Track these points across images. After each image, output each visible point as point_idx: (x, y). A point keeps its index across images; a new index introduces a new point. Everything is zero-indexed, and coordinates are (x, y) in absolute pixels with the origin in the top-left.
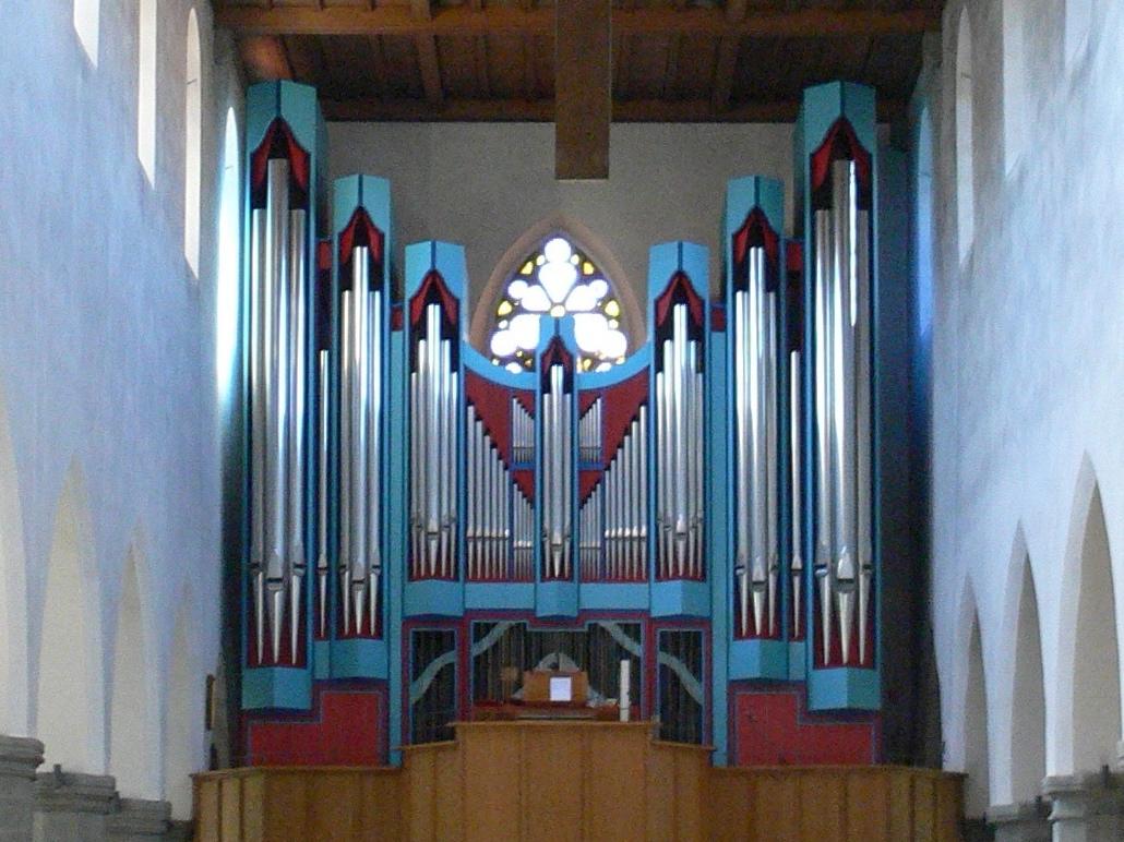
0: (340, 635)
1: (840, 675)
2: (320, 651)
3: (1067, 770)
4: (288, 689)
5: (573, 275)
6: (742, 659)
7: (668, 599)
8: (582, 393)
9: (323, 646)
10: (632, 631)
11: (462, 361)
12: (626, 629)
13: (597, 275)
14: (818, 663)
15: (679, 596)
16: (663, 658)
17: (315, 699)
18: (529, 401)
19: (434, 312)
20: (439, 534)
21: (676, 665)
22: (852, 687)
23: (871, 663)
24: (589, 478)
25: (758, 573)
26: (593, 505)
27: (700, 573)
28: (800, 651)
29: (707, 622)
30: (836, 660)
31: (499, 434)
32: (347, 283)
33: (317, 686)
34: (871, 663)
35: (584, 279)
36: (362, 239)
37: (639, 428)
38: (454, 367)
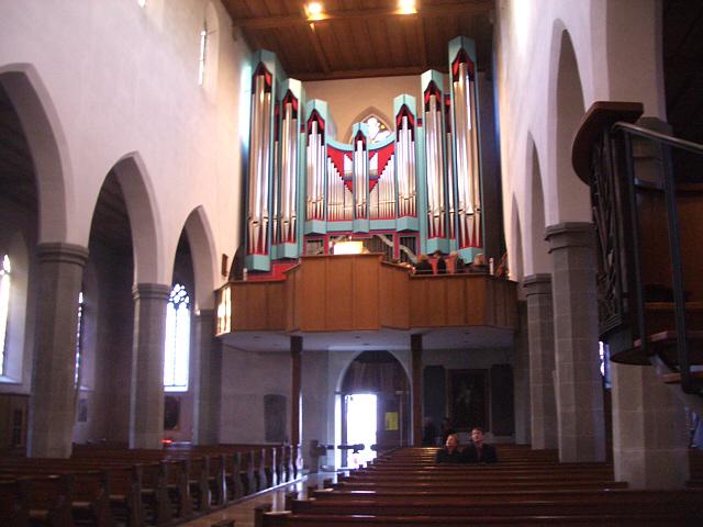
0: (281, 242)
1: (469, 250)
2: (273, 249)
3: (531, 273)
4: (261, 262)
5: (378, 129)
6: (430, 246)
7: (402, 224)
8: (370, 151)
9: (274, 247)
10: (389, 237)
11: (326, 142)
12: (387, 236)
13: (386, 129)
14: (461, 246)
15: (436, 244)
16: (401, 247)
17: (271, 267)
18: (350, 154)
19: (314, 124)
20: (316, 203)
21: (406, 250)
22: (439, 244)
23: (481, 246)
24: (373, 181)
25: (470, 211)
26: (374, 191)
27: (416, 215)
28: (454, 243)
29: (417, 232)
30: (467, 245)
31: (339, 167)
32: (284, 118)
33: (272, 262)
34: (481, 246)
35: (381, 131)
36: (290, 101)
37: (391, 163)
38: (323, 144)
